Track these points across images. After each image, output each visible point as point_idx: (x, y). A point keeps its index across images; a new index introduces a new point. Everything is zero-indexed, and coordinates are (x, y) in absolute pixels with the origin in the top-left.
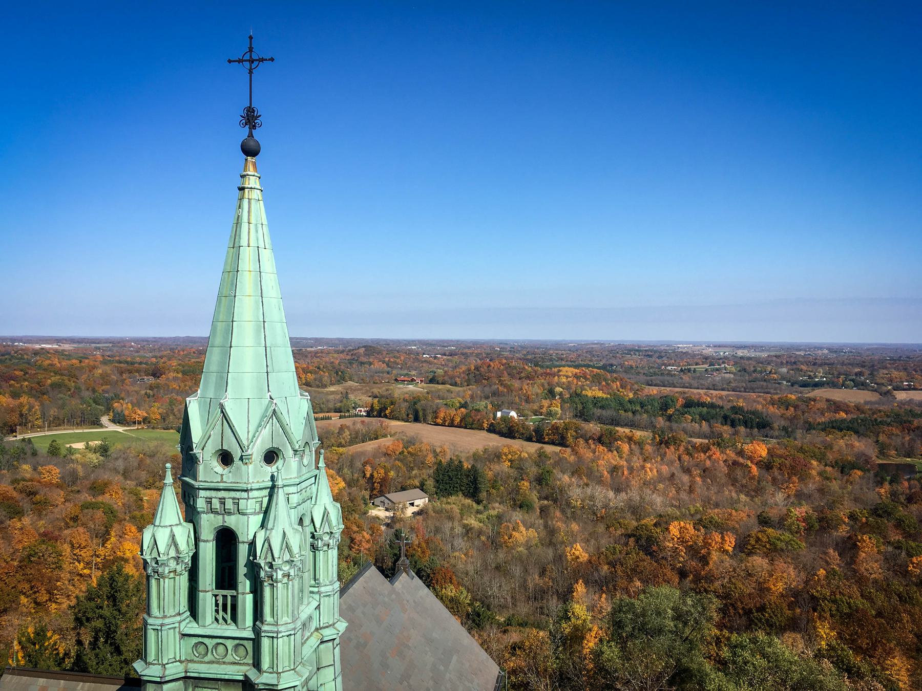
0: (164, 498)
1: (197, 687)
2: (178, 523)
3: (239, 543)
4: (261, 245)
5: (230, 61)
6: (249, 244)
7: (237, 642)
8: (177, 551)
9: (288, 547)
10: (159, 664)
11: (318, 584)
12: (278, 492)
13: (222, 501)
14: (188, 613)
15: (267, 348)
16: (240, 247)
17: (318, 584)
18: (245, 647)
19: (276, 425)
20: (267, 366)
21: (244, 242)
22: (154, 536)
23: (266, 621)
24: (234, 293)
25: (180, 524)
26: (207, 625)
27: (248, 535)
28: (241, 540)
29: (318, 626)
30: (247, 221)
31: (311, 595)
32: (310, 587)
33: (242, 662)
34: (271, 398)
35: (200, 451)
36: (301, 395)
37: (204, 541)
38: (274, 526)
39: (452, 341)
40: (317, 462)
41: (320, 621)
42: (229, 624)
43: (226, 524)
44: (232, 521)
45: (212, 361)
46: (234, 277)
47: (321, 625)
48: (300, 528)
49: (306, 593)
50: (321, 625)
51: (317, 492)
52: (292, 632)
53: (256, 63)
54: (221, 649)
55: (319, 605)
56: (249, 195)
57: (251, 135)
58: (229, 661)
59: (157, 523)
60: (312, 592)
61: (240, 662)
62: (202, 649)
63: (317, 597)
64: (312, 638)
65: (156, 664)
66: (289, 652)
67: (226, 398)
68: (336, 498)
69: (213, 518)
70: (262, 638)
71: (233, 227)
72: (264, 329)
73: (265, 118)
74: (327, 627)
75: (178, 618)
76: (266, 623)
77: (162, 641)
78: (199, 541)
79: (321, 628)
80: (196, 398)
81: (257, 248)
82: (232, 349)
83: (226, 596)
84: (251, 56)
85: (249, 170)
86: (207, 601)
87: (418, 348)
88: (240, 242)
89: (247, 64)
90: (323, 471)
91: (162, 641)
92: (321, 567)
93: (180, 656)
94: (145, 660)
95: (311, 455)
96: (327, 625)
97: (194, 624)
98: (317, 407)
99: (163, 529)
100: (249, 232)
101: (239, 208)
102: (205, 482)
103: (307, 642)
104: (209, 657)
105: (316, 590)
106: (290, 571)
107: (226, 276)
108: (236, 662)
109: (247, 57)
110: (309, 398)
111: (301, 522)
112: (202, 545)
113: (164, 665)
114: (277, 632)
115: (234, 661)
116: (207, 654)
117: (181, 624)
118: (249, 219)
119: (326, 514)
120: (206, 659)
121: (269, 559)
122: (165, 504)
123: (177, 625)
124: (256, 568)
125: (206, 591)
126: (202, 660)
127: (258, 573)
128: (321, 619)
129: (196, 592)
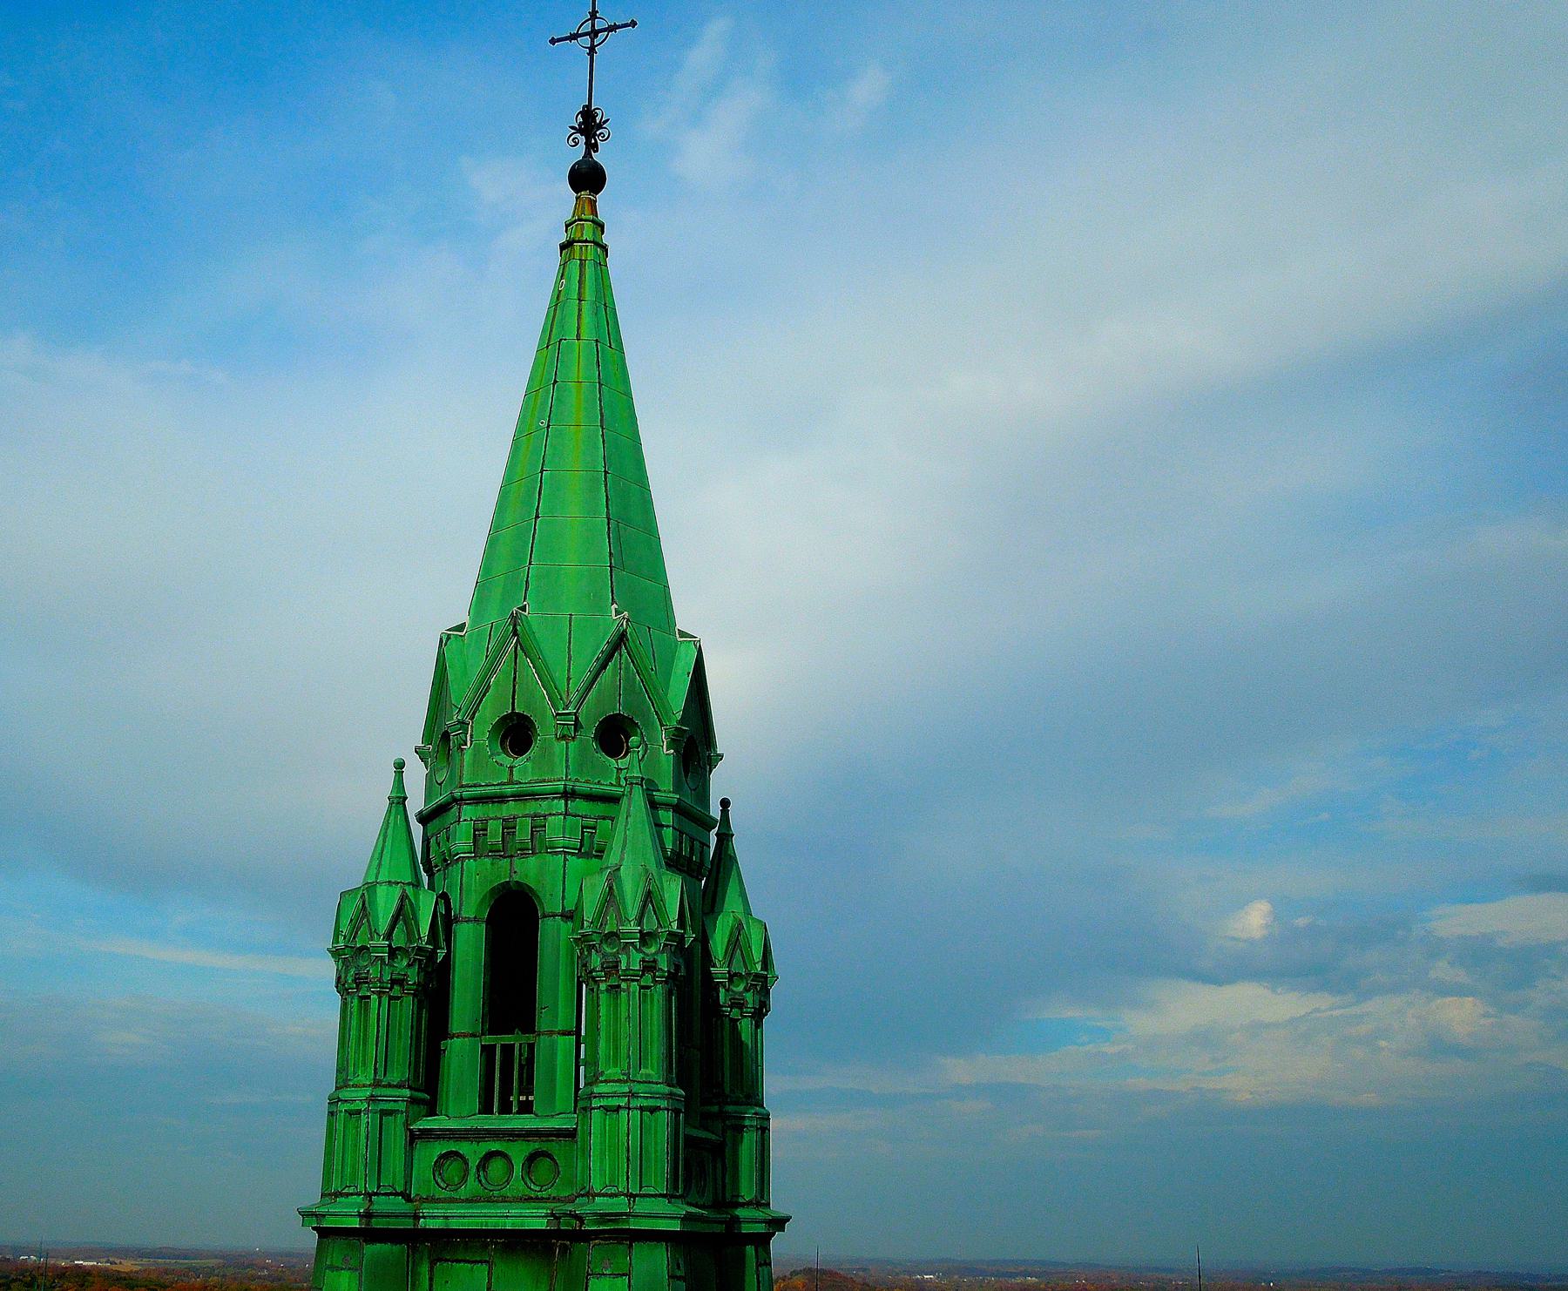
1: (440, 1260)
5: (553, 41)
7: (535, 1146)
10: (359, 1194)
13: (509, 825)
18: (553, 1159)
19: (627, 668)
30: (576, 297)
33: (544, 1195)
37: (468, 920)
43: (516, 878)
44: (528, 870)
46: (552, 359)
53: (602, 36)
54: (496, 1166)
56: (581, 254)
62: (452, 1169)
65: (352, 1194)
69: (489, 866)
83: (515, 828)
84: (593, 25)
89: (586, 41)
100: (579, 316)
102: (475, 786)
104: (471, 1186)
106: (658, 958)
108: (533, 1195)
109: (587, 27)
115: (527, 1192)
116: (464, 1179)
118: (580, 294)
120: (463, 1192)
126: (453, 1195)
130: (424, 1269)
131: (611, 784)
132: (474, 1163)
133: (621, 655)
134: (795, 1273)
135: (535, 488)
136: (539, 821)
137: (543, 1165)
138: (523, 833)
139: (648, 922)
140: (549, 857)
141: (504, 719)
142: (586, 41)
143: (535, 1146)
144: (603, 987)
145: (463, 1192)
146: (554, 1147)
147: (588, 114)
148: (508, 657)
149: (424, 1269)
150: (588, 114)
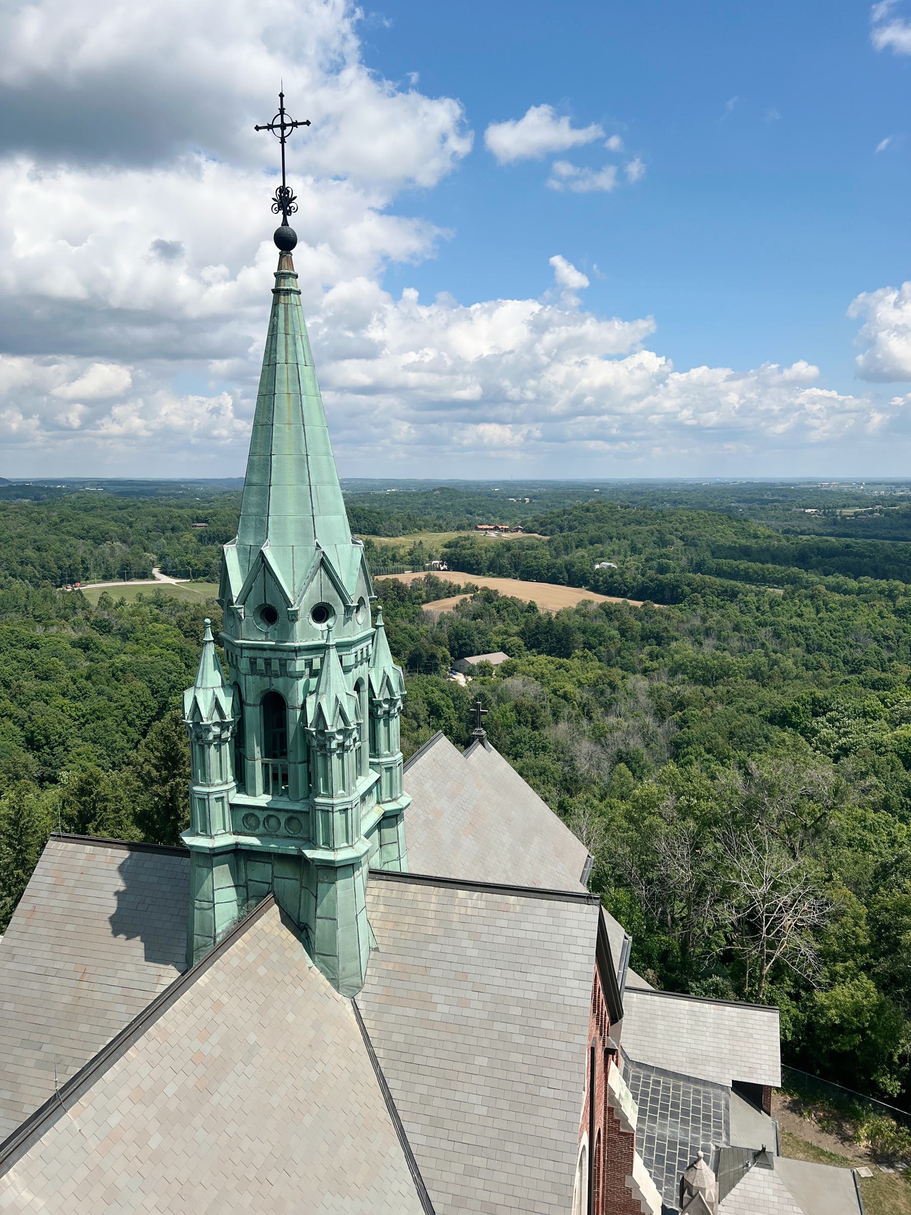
6: (286, 360)
9: (342, 714)
13: (268, 662)
28: (290, 703)
30: (283, 332)
34: (318, 545)
35: (241, 606)
36: (354, 542)
37: (250, 705)
38: (325, 691)
43: (273, 687)
50: (383, 800)
53: (289, 129)
54: (273, 822)
57: (285, 223)
62: (252, 821)
67: (267, 545)
72: (308, 463)
82: (271, 488)
90: (382, 630)
107: (262, 401)
109: (278, 122)
110: (363, 545)
114: (332, 806)
115: (288, 834)
118: (286, 329)
123: (224, 794)
126: (253, 832)
130: (242, 863)
132: (262, 819)
134: (434, 490)
135: (211, 928)
136: (283, 662)
137: (294, 823)
138: (275, 666)
140: (289, 679)
141: (260, 606)
143: (291, 814)
144: (319, 754)
145: (257, 831)
146: (299, 816)
147: (283, 190)
148: (261, 574)
149: (242, 863)
150: (283, 190)
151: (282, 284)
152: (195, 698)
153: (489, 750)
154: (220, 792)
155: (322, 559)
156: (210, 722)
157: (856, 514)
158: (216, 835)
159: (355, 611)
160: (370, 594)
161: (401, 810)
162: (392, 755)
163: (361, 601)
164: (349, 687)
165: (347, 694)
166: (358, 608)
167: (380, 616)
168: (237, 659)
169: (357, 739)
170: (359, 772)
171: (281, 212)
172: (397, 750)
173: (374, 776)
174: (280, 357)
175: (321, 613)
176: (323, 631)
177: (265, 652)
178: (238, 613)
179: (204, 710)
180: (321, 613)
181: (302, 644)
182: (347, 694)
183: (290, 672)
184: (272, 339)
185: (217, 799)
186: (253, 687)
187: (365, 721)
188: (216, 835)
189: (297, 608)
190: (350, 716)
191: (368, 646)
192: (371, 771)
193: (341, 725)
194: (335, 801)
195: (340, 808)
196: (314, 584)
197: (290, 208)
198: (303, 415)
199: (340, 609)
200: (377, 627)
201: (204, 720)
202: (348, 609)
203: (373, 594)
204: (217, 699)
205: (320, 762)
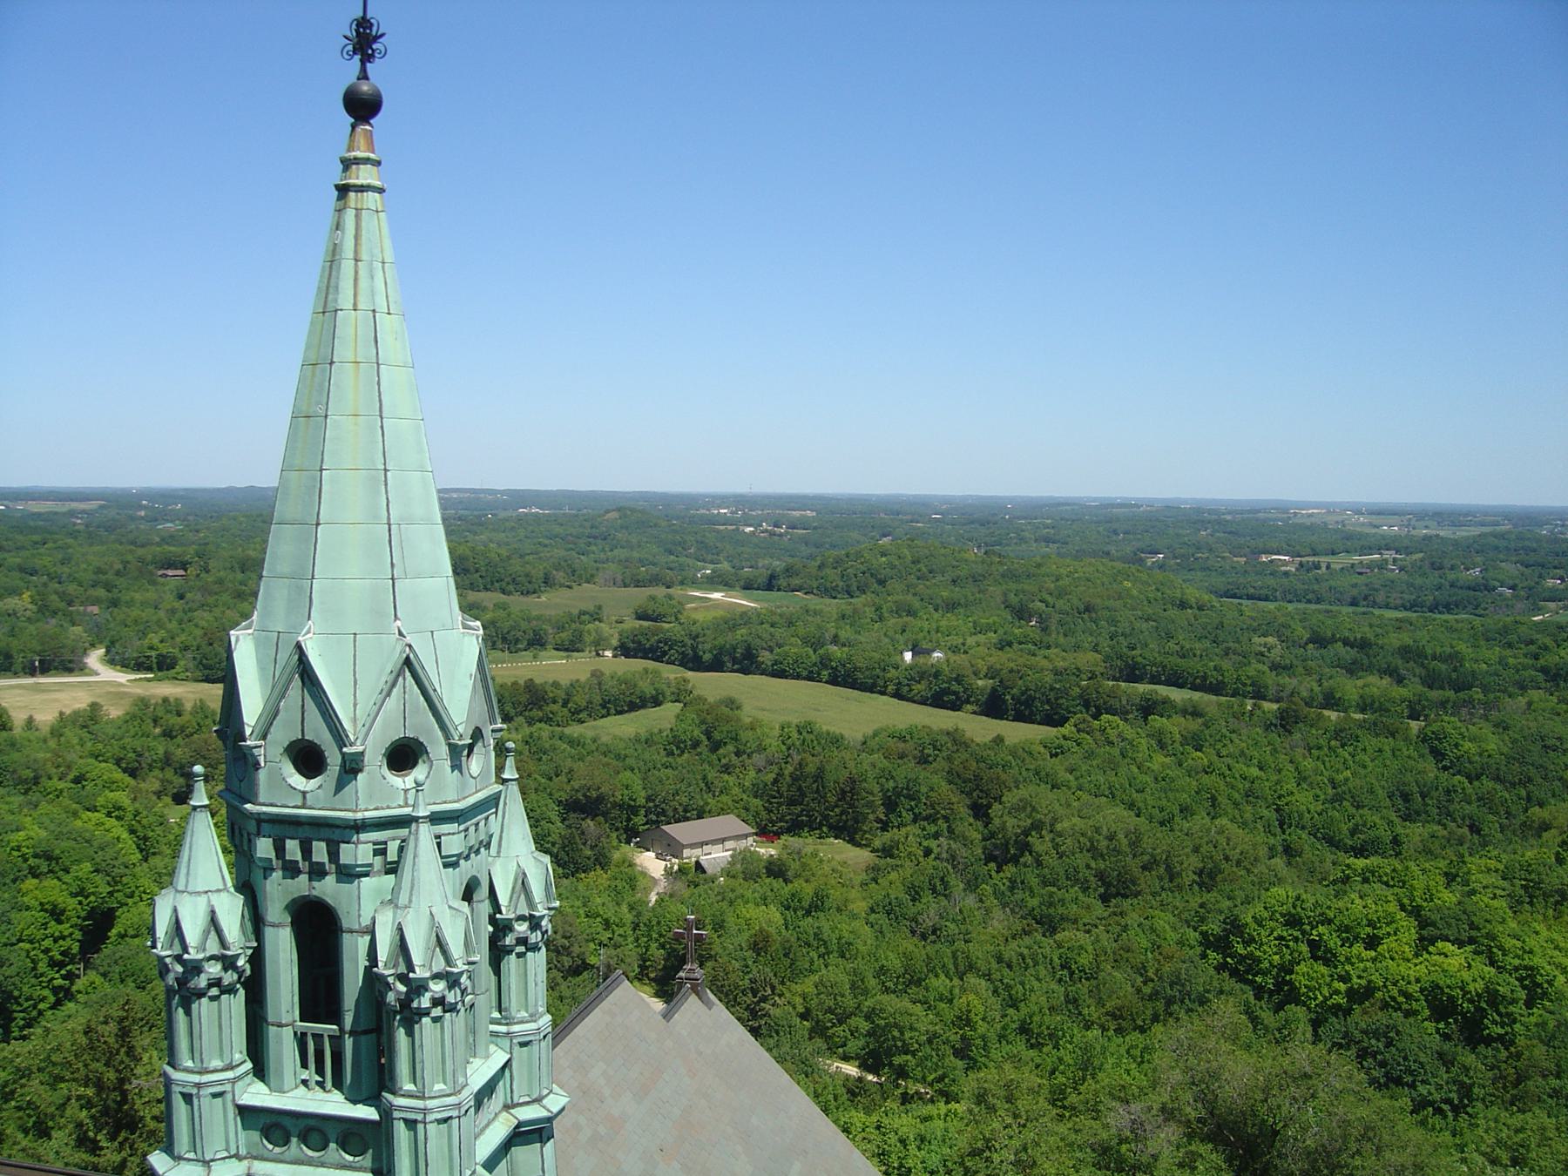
0: (192, 836)
2: (221, 887)
3: (342, 932)
4: (381, 305)
6: (355, 304)
8: (223, 943)
9: (441, 944)
11: (506, 1018)
12: (417, 830)
14: (249, 1065)
15: (393, 527)
16: (336, 311)
17: (506, 1018)
19: (411, 685)
20: (392, 565)
21: (345, 300)
22: (175, 910)
23: (401, 1088)
24: (324, 408)
25: (226, 889)
26: (286, 1089)
27: (359, 916)
28: (345, 924)
29: (509, 1101)
30: (351, 255)
31: (494, 1039)
32: (491, 1023)
34: (401, 634)
35: (259, 743)
36: (465, 627)
37: (274, 925)
38: (410, 901)
39: (805, 497)
40: (500, 769)
41: (512, 1092)
42: (329, 1091)
43: (314, 893)
44: (328, 888)
45: (280, 551)
47: (515, 1101)
48: (464, 906)
49: (483, 1037)
50: (515, 1101)
51: (502, 832)
52: (455, 1113)
55: (510, 1060)
57: (364, 76)
58: (332, 1161)
59: (181, 887)
60: (494, 1034)
61: (353, 1165)
63: (506, 1042)
64: (496, 1123)
66: (450, 1150)
67: (308, 632)
68: (541, 842)
70: (395, 1122)
71: (323, 271)
72: (386, 485)
73: (391, 42)
74: (527, 1103)
75: (230, 1075)
76: (402, 1093)
77: (200, 1117)
78: (264, 925)
79: (515, 1106)
80: (250, 631)
81: (371, 314)
82: (320, 528)
85: (359, 149)
86: (283, 1045)
87: (732, 513)
88: (336, 300)
90: (514, 788)
91: (200, 1117)
92: (513, 987)
93: (238, 1147)
94: (169, 1149)
95: (487, 753)
96: (528, 1099)
97: (260, 1086)
98: (499, 639)
99: (193, 898)
100: (356, 280)
101: (337, 229)
103: (487, 1131)
105: (503, 1029)
107: (309, 374)
110: (481, 632)
111: (468, 895)
112: (269, 932)
113: (208, 1162)
114: (425, 1111)
117: (236, 1085)
118: (356, 252)
119: (523, 884)
121: (402, 969)
122: (194, 847)
123: (228, 1087)
124: (377, 984)
125: (280, 1025)
127: (383, 996)
128: (514, 1087)
129: (262, 1027)
131: (400, 807)
133: (404, 679)
139: (436, 962)
142: (463, 834)
147: (363, 23)
150: (363, 23)
151: (353, 176)
152: (175, 910)
153: (709, 1005)
154: (220, 1082)
155: (408, 658)
156: (201, 956)
157: (469, 497)
158: (213, 1160)
159: (465, 753)
160: (492, 721)
161: (549, 1120)
162: (533, 1018)
163: (477, 734)
164: (454, 897)
165: (450, 907)
166: (471, 748)
167: (510, 762)
168: (250, 841)
169: (469, 990)
170: (473, 1050)
171: (357, 57)
172: (541, 1009)
173: (499, 1058)
174: (345, 299)
175: (403, 756)
176: (406, 791)
177: (300, 829)
178: (253, 755)
179: (192, 934)
180: (403, 756)
181: (368, 814)
182: (450, 907)
183: (346, 866)
184: (331, 267)
185: (215, 1095)
186: (278, 892)
187: (482, 955)
188: (213, 1160)
189: (360, 749)
190: (456, 950)
191: (477, 825)
192: (492, 1048)
193: (439, 965)
194: (430, 1104)
195: (439, 1116)
196: (392, 703)
197: (373, 51)
198: (380, 401)
199: (439, 750)
200: (504, 781)
201: (191, 950)
202: (454, 751)
203: (499, 720)
204: (213, 912)
205: (401, 1034)
